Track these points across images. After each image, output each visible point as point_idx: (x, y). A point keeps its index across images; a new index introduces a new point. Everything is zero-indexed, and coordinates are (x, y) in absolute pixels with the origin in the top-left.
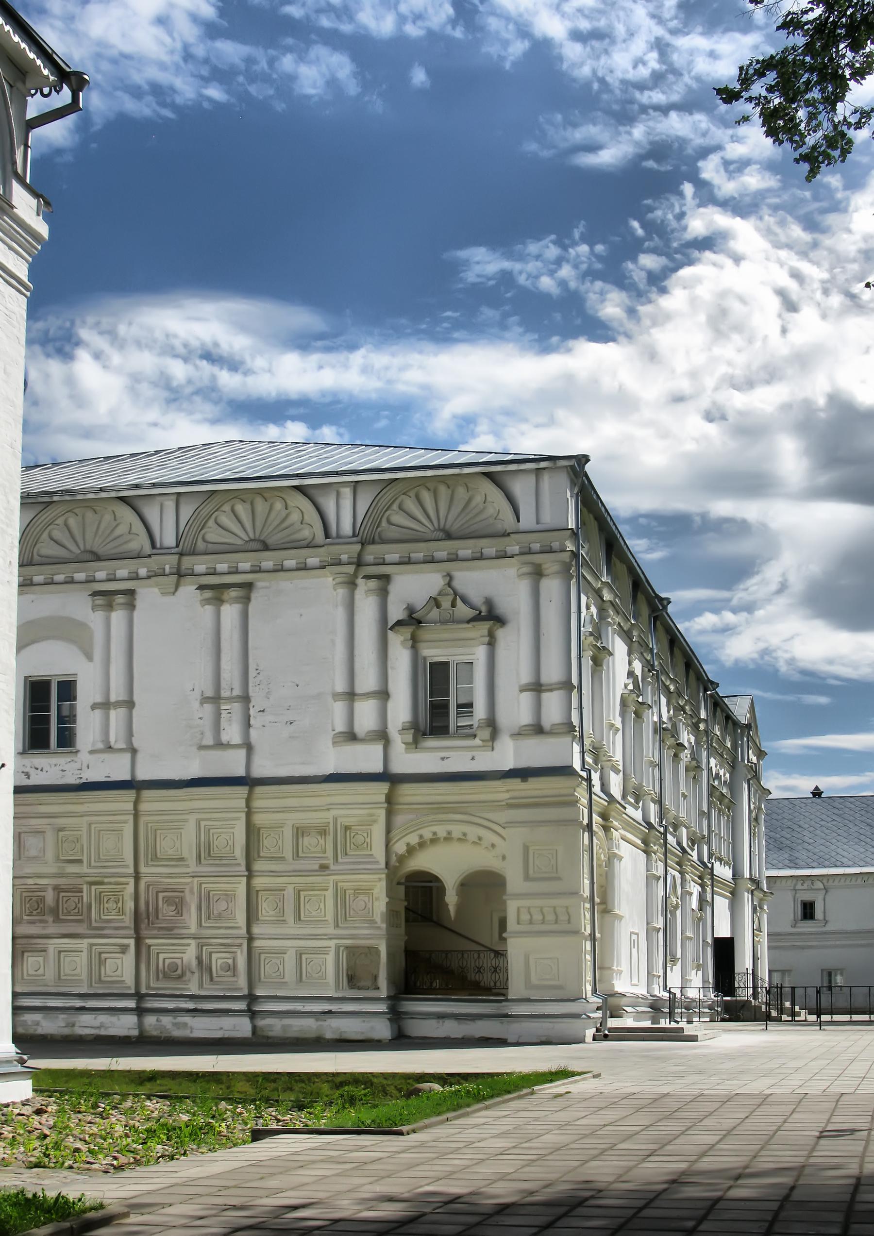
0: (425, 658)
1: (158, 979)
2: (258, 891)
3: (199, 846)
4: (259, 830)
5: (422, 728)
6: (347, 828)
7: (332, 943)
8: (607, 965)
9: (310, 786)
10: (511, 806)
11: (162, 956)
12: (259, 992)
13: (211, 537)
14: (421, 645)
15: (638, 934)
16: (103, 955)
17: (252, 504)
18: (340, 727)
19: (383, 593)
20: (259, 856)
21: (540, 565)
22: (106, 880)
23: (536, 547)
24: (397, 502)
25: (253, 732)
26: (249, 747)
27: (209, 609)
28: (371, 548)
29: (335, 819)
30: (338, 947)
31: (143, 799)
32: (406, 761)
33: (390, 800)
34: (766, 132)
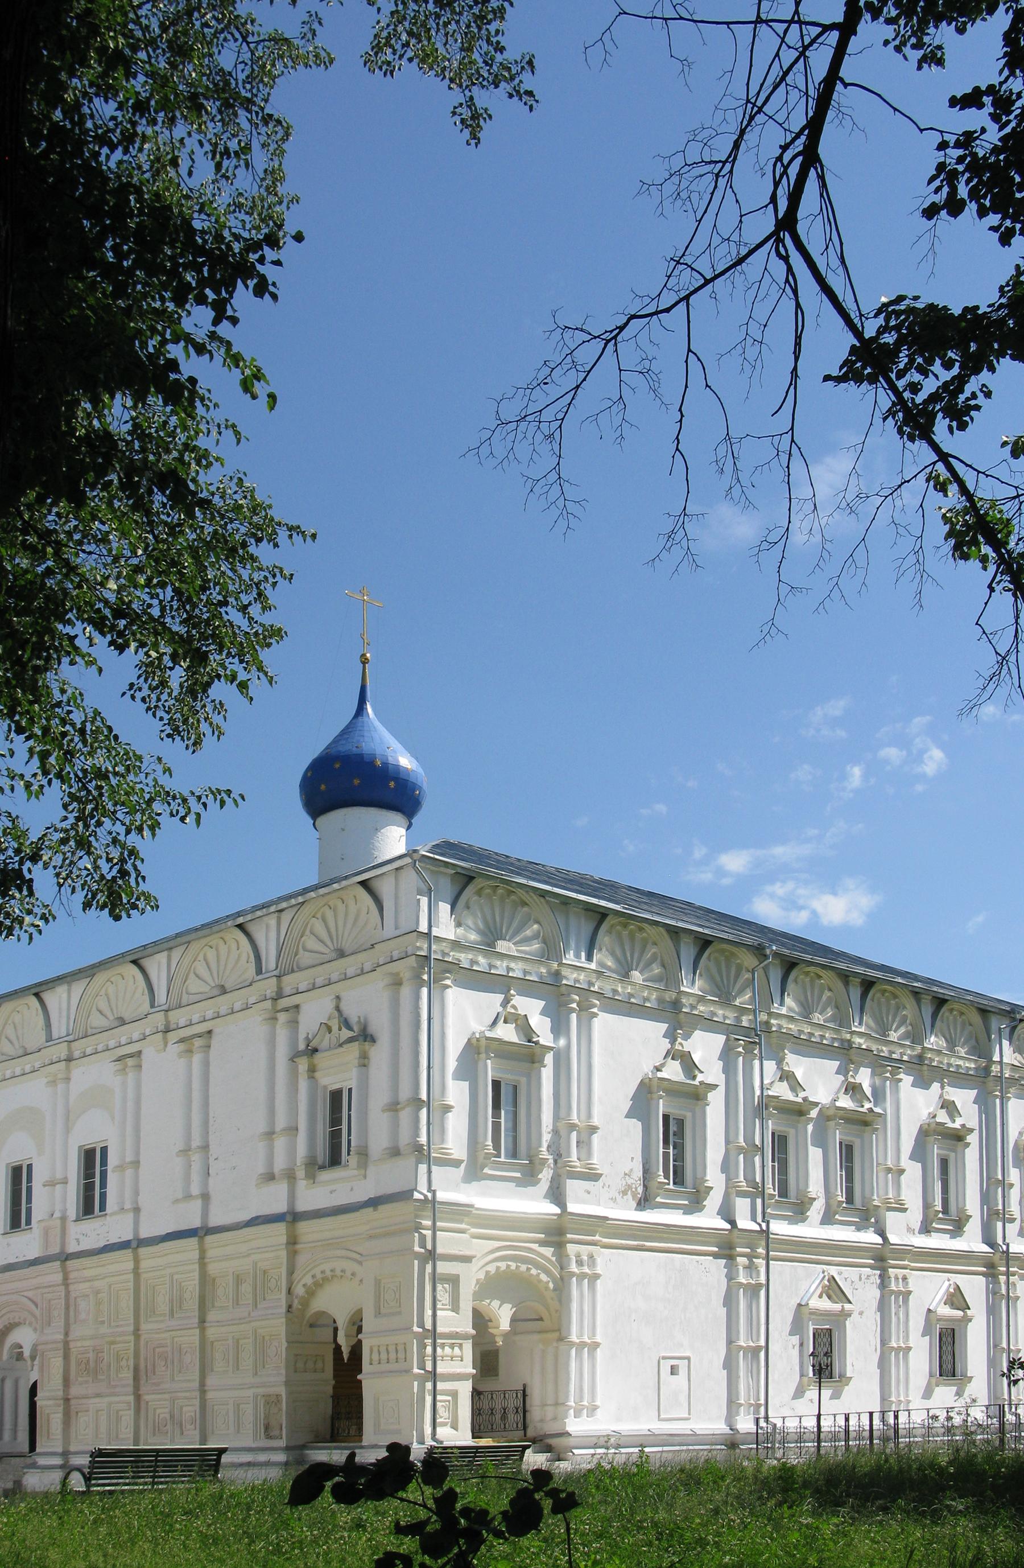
0: (325, 1087)
1: (154, 1435)
2: (212, 1342)
3: (171, 1301)
4: (214, 1280)
5: (320, 1160)
6: (265, 1272)
7: (250, 1393)
8: (561, 1401)
9: (218, 1235)
10: (371, 1237)
11: (158, 1411)
12: (72, 1448)
13: (193, 989)
14: (317, 1075)
15: (688, 1359)
16: (121, 1413)
17: (217, 950)
18: (261, 1169)
19: (294, 1023)
20: (213, 1306)
21: (398, 974)
22: (118, 1339)
23: (335, 977)
24: (94, 1008)
25: (211, 1181)
26: (205, 1197)
27: (183, 1062)
28: (286, 979)
29: (255, 1264)
30: (255, 1396)
31: (142, 1257)
32: (312, 1196)
33: (292, 1241)
34: (949, 213)
